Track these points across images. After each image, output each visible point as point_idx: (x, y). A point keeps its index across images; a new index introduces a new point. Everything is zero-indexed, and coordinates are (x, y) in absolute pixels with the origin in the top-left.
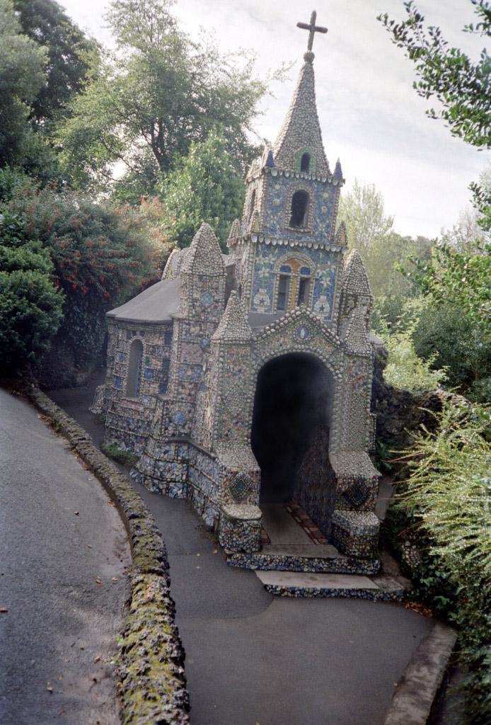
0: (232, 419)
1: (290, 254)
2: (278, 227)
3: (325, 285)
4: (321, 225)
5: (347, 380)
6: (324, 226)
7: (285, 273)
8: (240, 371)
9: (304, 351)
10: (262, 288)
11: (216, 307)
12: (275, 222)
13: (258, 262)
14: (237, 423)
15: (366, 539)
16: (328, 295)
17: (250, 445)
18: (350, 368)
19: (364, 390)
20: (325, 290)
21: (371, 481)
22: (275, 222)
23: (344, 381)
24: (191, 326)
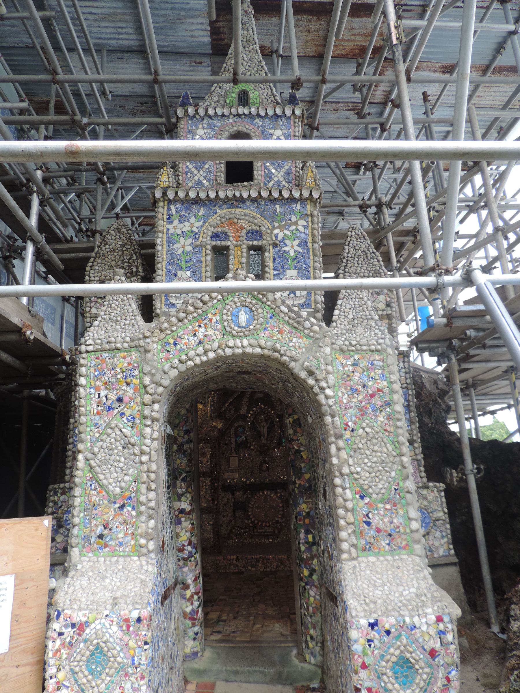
1: (224, 212)
3: (292, 253)
5: (345, 401)
7: (218, 243)
9: (249, 350)
10: (181, 269)
13: (171, 232)
14: (122, 507)
18: (348, 377)
19: (389, 418)
21: (432, 631)
23: (339, 402)
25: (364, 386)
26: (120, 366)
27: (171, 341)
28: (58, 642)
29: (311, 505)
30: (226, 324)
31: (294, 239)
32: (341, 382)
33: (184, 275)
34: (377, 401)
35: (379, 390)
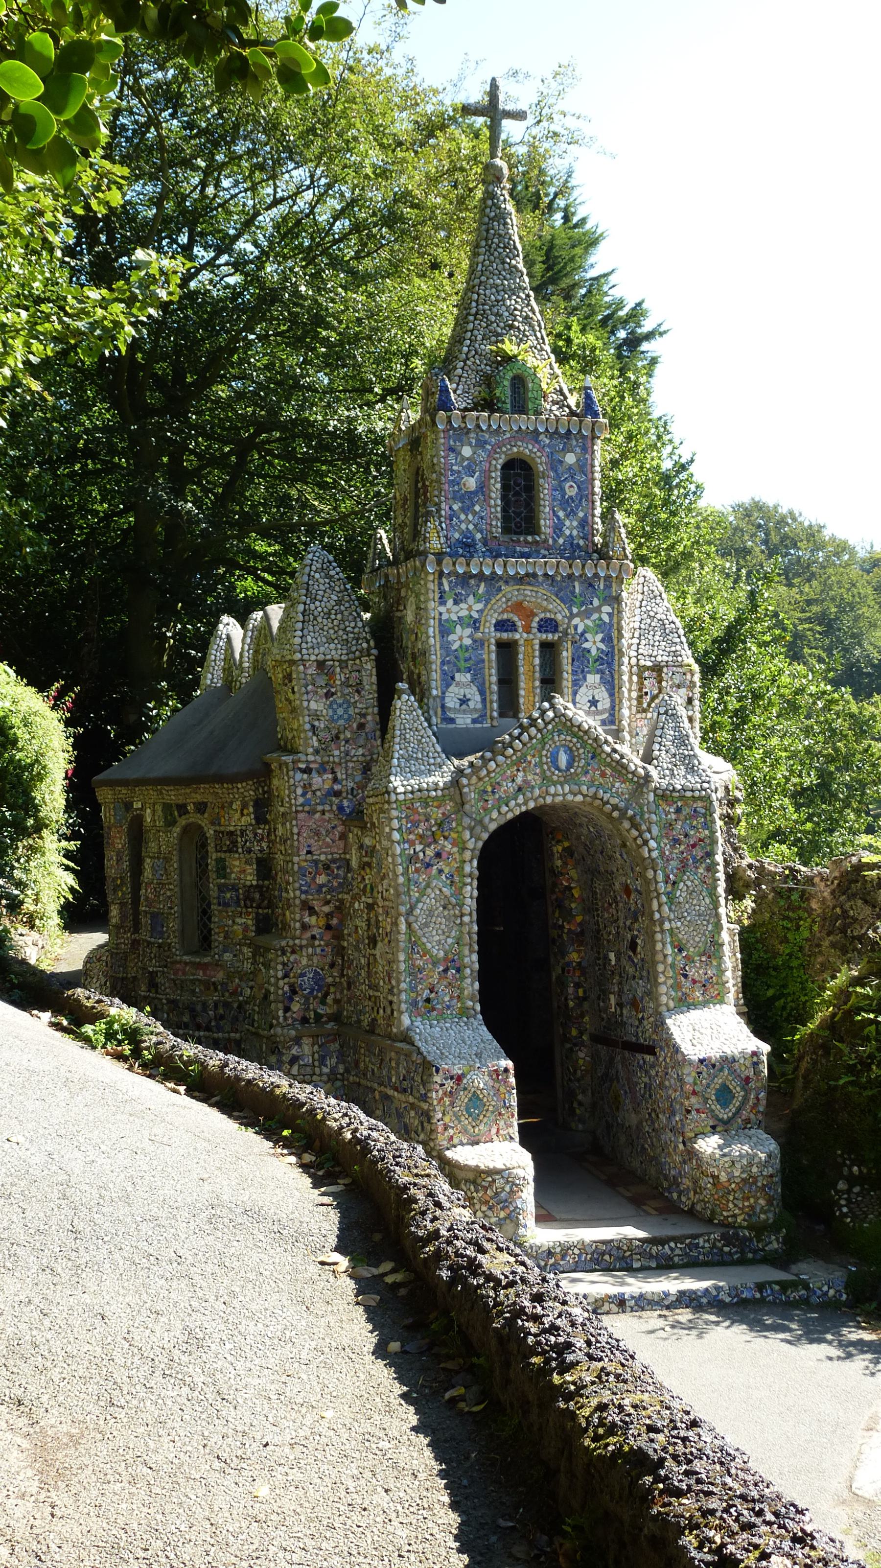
0: (435, 964)
2: (478, 536)
4: (567, 523)
6: (575, 523)
7: (505, 636)
8: (438, 855)
9: (570, 797)
10: (459, 671)
11: (361, 726)
12: (471, 527)
13: (444, 617)
14: (446, 971)
15: (755, 1183)
16: (602, 672)
17: (480, 1017)
18: (670, 825)
20: (596, 661)
21: (748, 1063)
22: (471, 527)
23: (662, 854)
24: (314, 774)
25: (686, 836)
26: (434, 816)
27: (489, 789)
28: (441, 1092)
29: (583, 954)
30: (545, 767)
31: (597, 633)
32: (664, 831)
33: (463, 679)
34: (698, 852)
35: (701, 840)
